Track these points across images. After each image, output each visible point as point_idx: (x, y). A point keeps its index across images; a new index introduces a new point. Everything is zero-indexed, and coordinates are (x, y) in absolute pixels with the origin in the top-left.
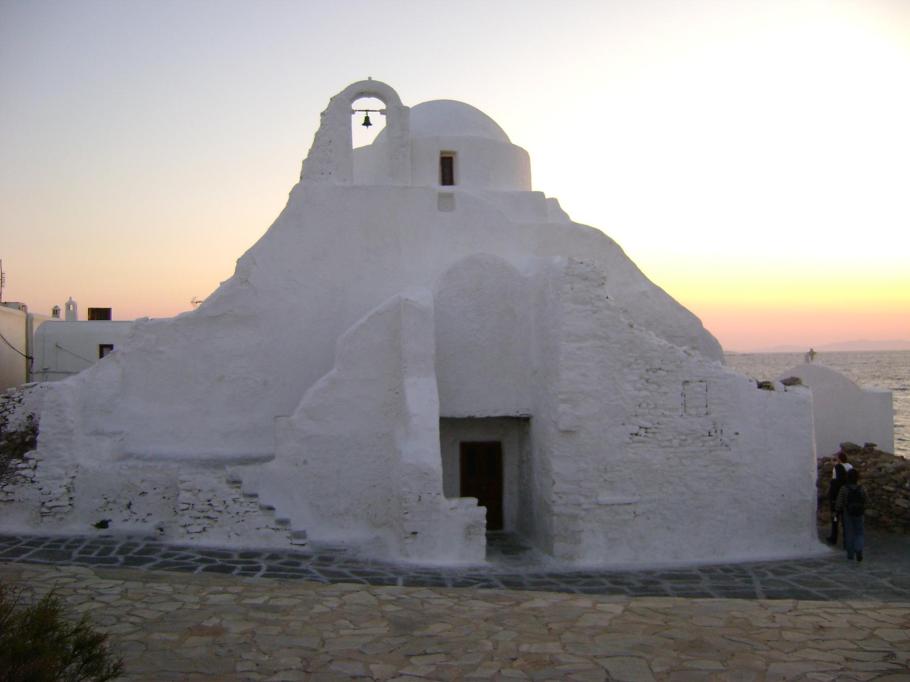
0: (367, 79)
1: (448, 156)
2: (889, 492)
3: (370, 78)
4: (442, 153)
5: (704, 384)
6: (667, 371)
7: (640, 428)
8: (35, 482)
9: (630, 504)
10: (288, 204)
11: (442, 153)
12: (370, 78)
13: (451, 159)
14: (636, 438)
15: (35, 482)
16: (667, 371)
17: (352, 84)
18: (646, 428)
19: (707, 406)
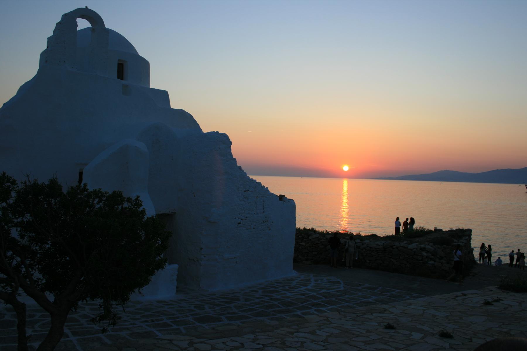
0: (85, 7)
1: (121, 63)
2: (303, 245)
3: (86, 7)
4: (119, 60)
5: (263, 198)
6: (251, 192)
7: (241, 220)
8: (240, 343)
9: (234, 258)
10: (39, 71)
11: (119, 60)
12: (86, 7)
13: (122, 65)
14: (240, 225)
15: (240, 343)
16: (251, 192)
17: (78, 9)
18: (243, 220)
19: (263, 209)
